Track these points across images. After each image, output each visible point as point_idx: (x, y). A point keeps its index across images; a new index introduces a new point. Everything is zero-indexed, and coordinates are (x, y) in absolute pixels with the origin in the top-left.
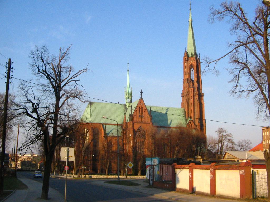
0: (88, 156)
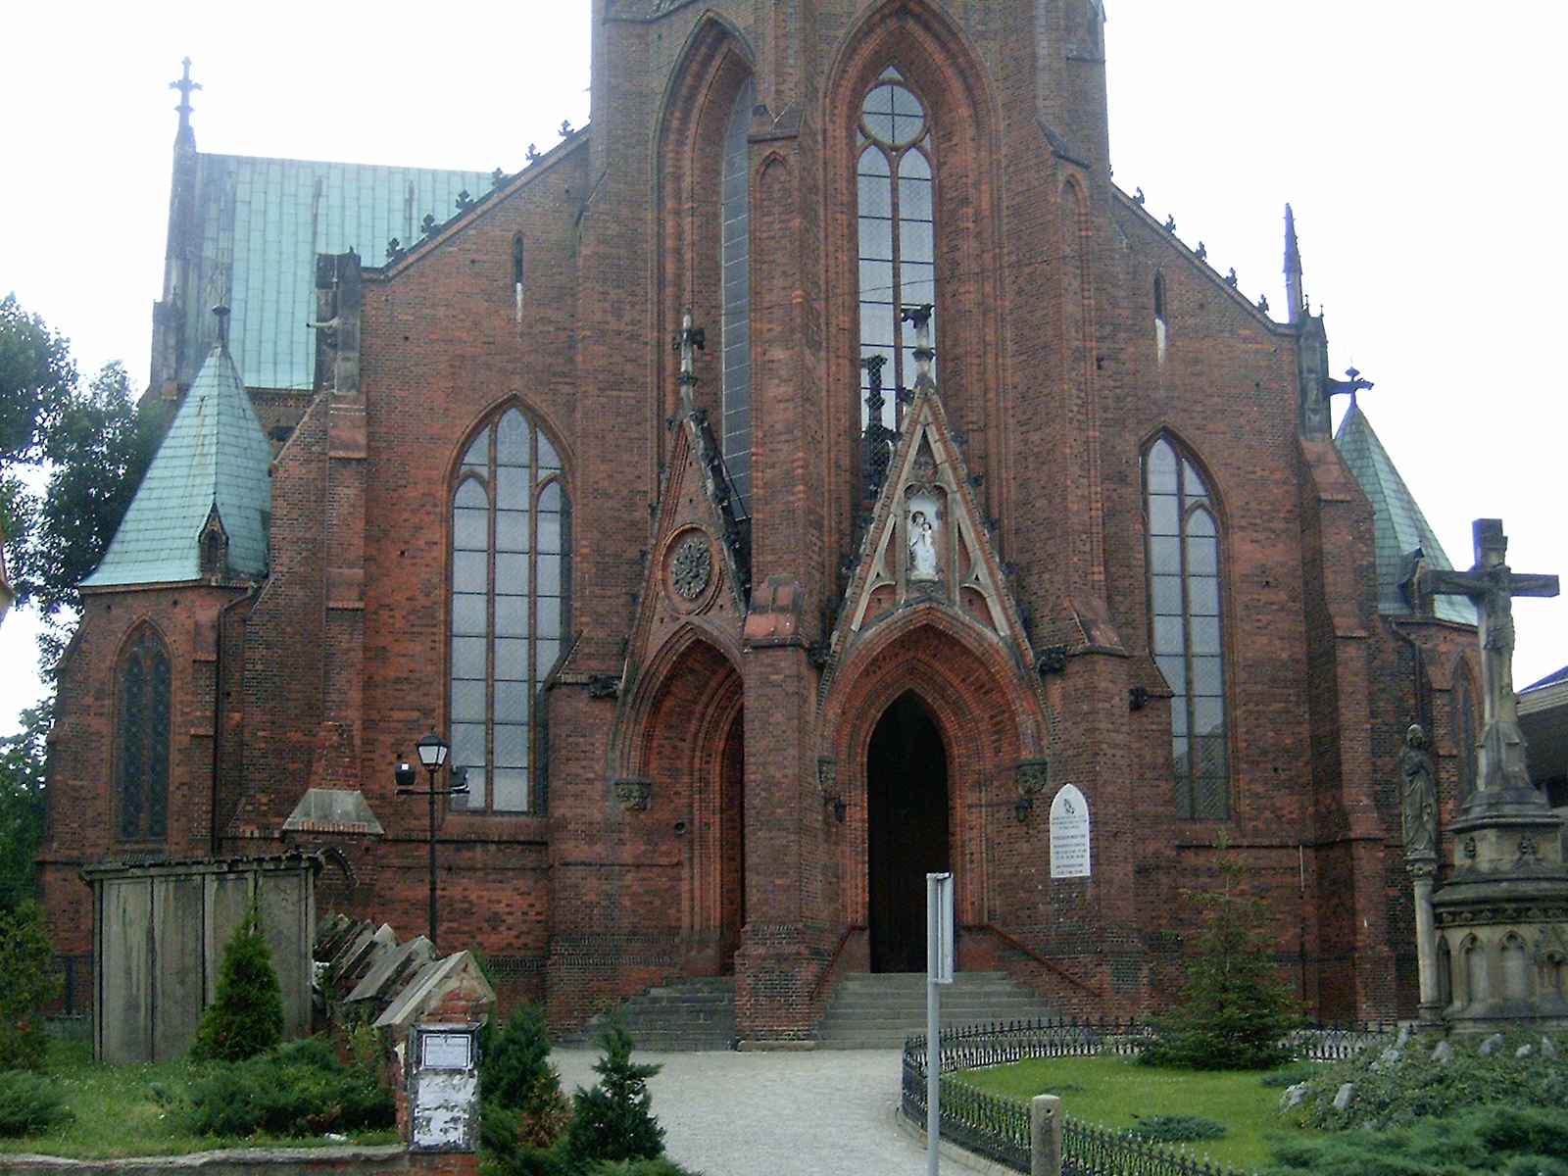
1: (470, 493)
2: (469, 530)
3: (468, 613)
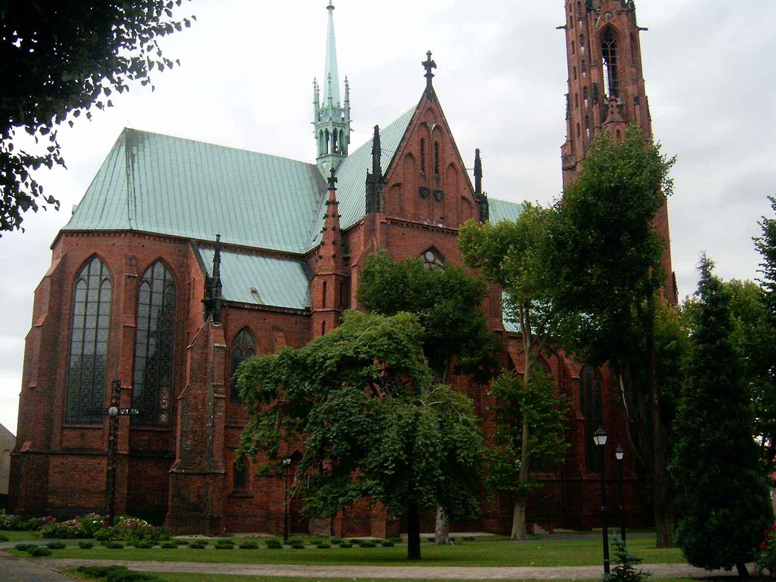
0: (524, 270)
1: (82, 285)
2: (80, 295)
3: (78, 321)
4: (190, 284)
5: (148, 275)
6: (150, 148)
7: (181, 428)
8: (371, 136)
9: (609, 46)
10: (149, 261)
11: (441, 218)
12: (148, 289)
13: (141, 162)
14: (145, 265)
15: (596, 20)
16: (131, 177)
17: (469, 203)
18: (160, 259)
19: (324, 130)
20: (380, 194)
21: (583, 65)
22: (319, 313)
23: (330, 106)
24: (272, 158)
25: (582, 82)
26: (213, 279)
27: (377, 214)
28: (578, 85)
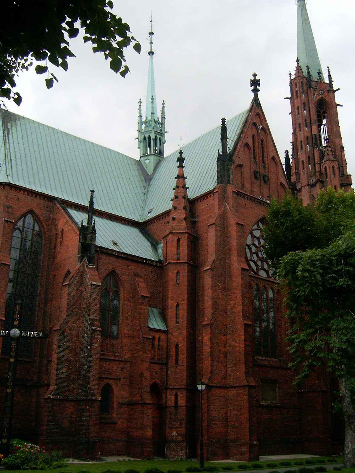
4: (57, 234)
5: (20, 223)
6: (21, 126)
7: (58, 357)
8: (220, 123)
9: (322, 112)
10: (22, 212)
11: (268, 197)
12: (20, 236)
13: (15, 135)
14: (18, 214)
15: (314, 94)
16: (7, 144)
17: (285, 188)
18: (31, 212)
19: (147, 136)
20: (230, 170)
21: (306, 123)
22: (173, 265)
23: (153, 119)
24: (110, 151)
25: (305, 133)
26: (87, 227)
27: (229, 184)
28: (302, 135)
